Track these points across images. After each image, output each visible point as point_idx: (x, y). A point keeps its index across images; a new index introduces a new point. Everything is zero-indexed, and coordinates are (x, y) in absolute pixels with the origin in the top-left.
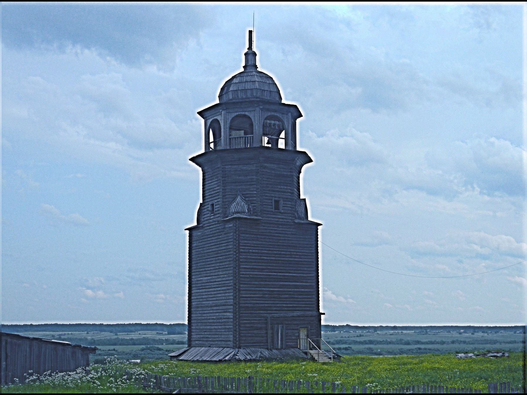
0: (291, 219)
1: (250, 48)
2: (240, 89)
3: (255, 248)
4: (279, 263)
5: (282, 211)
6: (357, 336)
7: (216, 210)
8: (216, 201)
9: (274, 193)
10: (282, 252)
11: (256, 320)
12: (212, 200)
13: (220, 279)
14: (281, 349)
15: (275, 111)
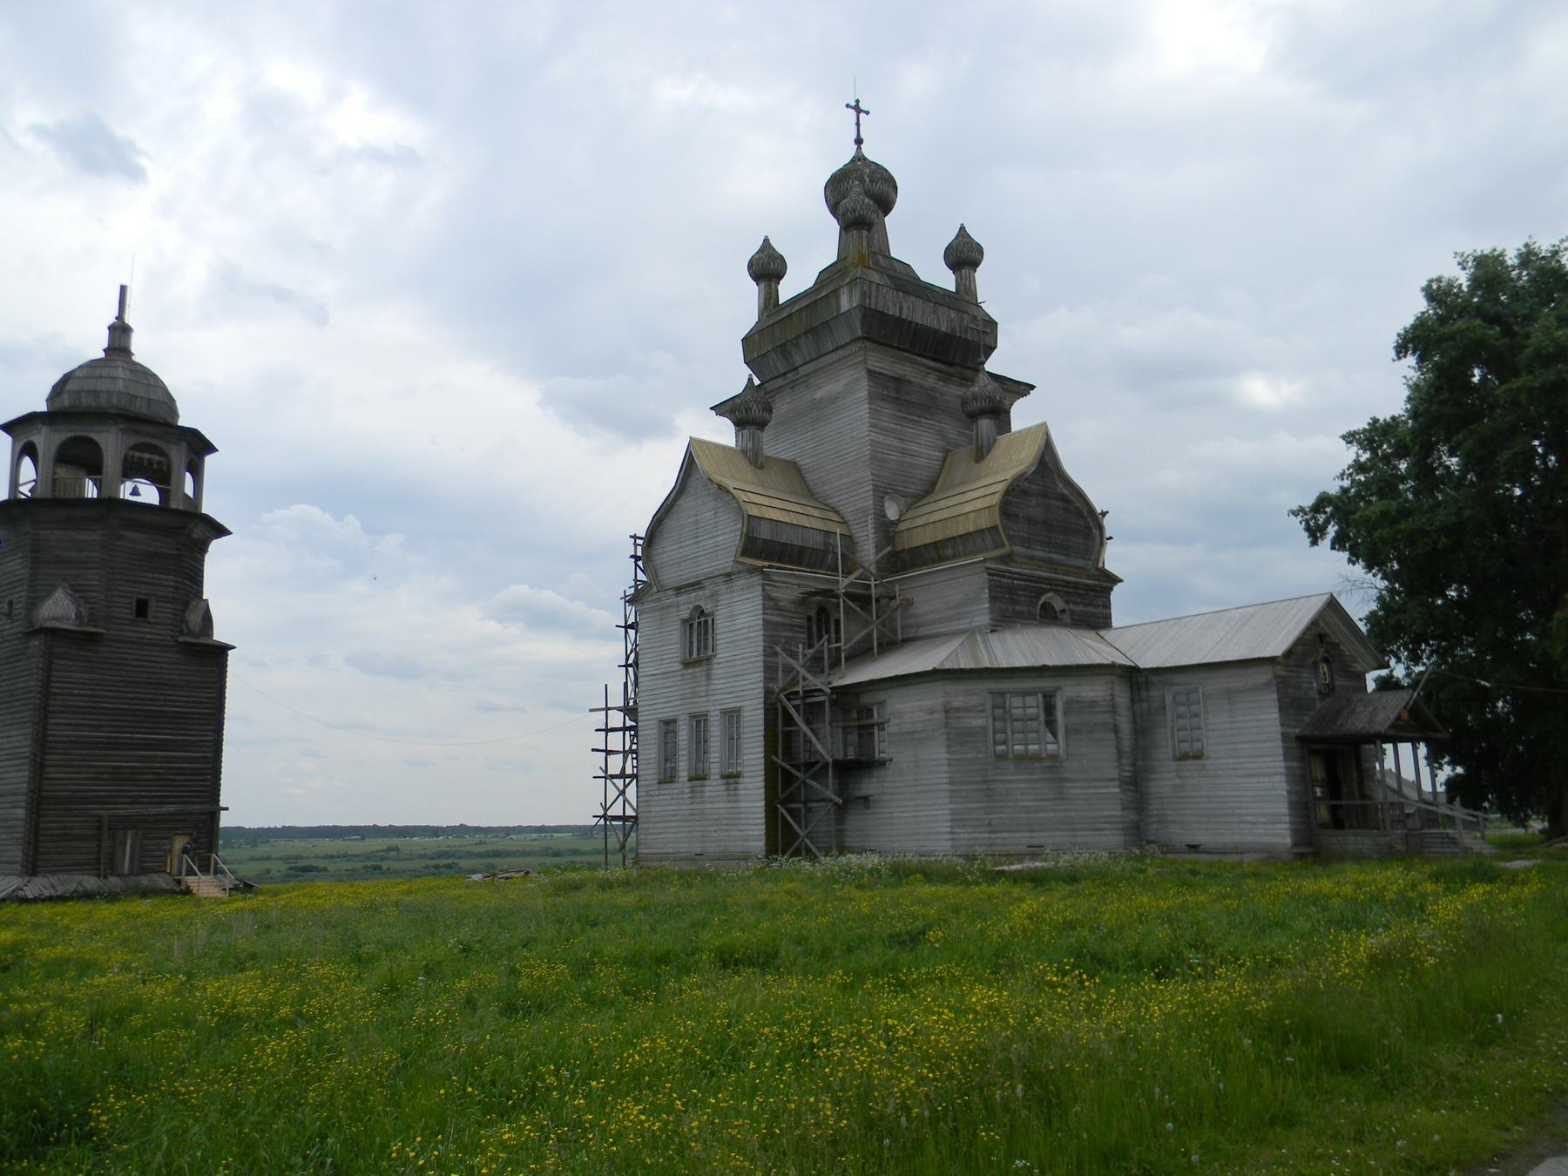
0: (172, 636)
1: (120, 317)
2: (86, 389)
3: (86, 687)
4: (138, 716)
5: (153, 620)
6: (476, 844)
7: (16, 612)
8: (17, 596)
9: (136, 585)
10: (147, 696)
11: (77, 822)
12: (12, 594)
13: (11, 745)
14: (128, 875)
15: (153, 436)
